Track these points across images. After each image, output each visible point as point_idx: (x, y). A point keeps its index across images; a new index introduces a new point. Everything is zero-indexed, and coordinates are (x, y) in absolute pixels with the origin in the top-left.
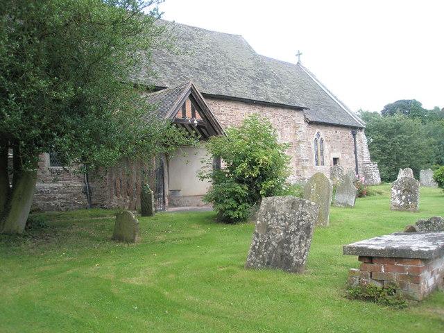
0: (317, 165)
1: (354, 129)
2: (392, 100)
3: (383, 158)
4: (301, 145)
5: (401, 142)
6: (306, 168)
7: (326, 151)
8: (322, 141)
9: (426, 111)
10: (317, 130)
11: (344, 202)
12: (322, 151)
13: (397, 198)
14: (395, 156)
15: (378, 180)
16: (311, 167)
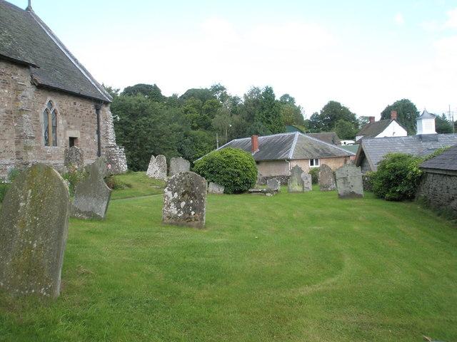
0: (46, 145)
1: (98, 103)
2: (132, 83)
3: (126, 141)
4: (25, 116)
5: (145, 125)
6: (30, 148)
7: (61, 127)
8: (55, 112)
9: (165, 98)
10: (49, 99)
11: (89, 209)
12: (55, 127)
13: (172, 204)
14: (138, 140)
15: (125, 167)
16: (38, 148)
